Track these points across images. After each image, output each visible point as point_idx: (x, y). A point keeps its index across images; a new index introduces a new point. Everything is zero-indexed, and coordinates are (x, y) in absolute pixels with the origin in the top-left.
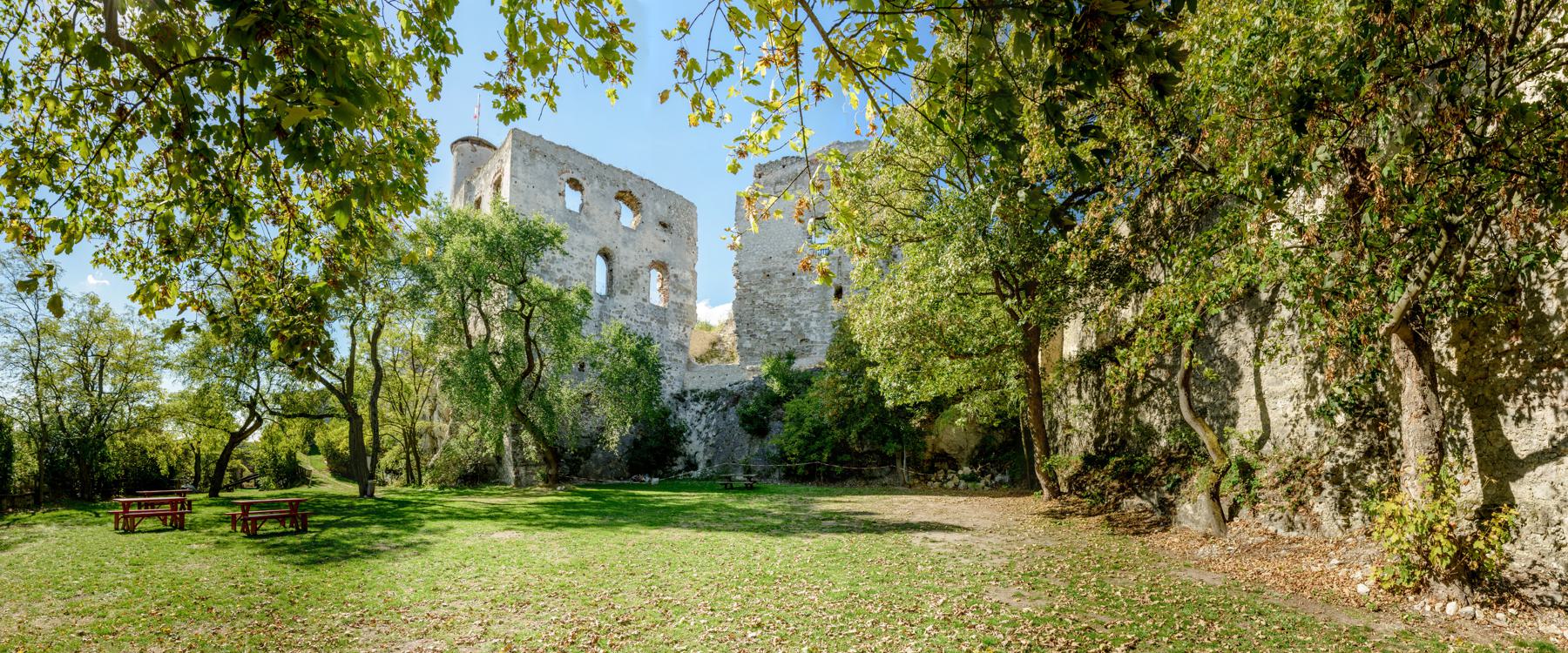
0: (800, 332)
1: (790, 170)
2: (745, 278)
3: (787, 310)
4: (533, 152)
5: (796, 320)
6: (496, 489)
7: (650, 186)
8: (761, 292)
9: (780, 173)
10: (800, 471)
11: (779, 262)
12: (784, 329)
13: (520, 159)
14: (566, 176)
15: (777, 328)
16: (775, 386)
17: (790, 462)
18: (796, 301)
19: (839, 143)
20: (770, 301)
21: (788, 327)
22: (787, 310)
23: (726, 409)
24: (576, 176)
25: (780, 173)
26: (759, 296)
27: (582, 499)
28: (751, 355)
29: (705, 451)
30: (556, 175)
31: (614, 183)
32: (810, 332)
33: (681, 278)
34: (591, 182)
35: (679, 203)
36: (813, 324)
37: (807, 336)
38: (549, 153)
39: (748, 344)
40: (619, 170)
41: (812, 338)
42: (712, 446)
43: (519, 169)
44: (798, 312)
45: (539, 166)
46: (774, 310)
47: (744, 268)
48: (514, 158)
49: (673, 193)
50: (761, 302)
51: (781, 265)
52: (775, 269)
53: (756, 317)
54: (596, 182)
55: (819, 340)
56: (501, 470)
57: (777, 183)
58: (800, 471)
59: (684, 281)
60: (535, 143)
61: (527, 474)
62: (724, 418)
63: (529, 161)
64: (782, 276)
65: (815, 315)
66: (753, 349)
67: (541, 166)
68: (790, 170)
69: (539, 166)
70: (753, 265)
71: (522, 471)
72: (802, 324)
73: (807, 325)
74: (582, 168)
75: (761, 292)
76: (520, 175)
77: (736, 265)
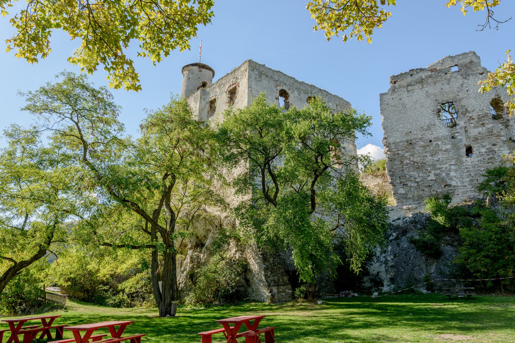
0: (443, 180)
1: (416, 77)
2: (393, 146)
3: (429, 166)
4: (261, 74)
5: (438, 172)
6: (252, 305)
7: (325, 94)
8: (407, 155)
9: (409, 79)
10: (489, 284)
11: (417, 134)
12: (429, 178)
13: (253, 77)
14: (279, 88)
15: (424, 179)
16: (440, 219)
17: (476, 277)
18: (436, 159)
19: (450, 57)
20: (415, 160)
21: (432, 177)
22: (429, 166)
23: (397, 238)
24: (285, 88)
25: (409, 79)
26: (406, 158)
27: (203, 315)
28: (406, 198)
29: (387, 271)
30: (274, 88)
31: (306, 92)
32: (451, 179)
33: (347, 149)
34: (293, 91)
35: (341, 102)
36: (452, 174)
37: (449, 182)
38: (269, 75)
39: (402, 191)
40: (308, 84)
41: (453, 183)
42: (392, 266)
43: (253, 83)
44: (438, 166)
45: (264, 81)
46: (419, 167)
47: (391, 140)
48: (250, 77)
49: (337, 97)
50: (408, 161)
51: (420, 136)
52: (415, 139)
53: (406, 172)
54: (296, 92)
55: (459, 184)
56: (250, 290)
57: (408, 85)
58: (489, 284)
59: (350, 151)
60: (262, 69)
61: (278, 292)
62: (398, 245)
63: (258, 79)
64: (422, 143)
65: (453, 167)
66: (406, 194)
67: (265, 82)
68: (416, 77)
69: (264, 81)
70: (397, 137)
71: (275, 290)
72: (444, 174)
73: (448, 175)
74: (288, 84)
75: (407, 155)
76: (254, 86)
77: (385, 138)
